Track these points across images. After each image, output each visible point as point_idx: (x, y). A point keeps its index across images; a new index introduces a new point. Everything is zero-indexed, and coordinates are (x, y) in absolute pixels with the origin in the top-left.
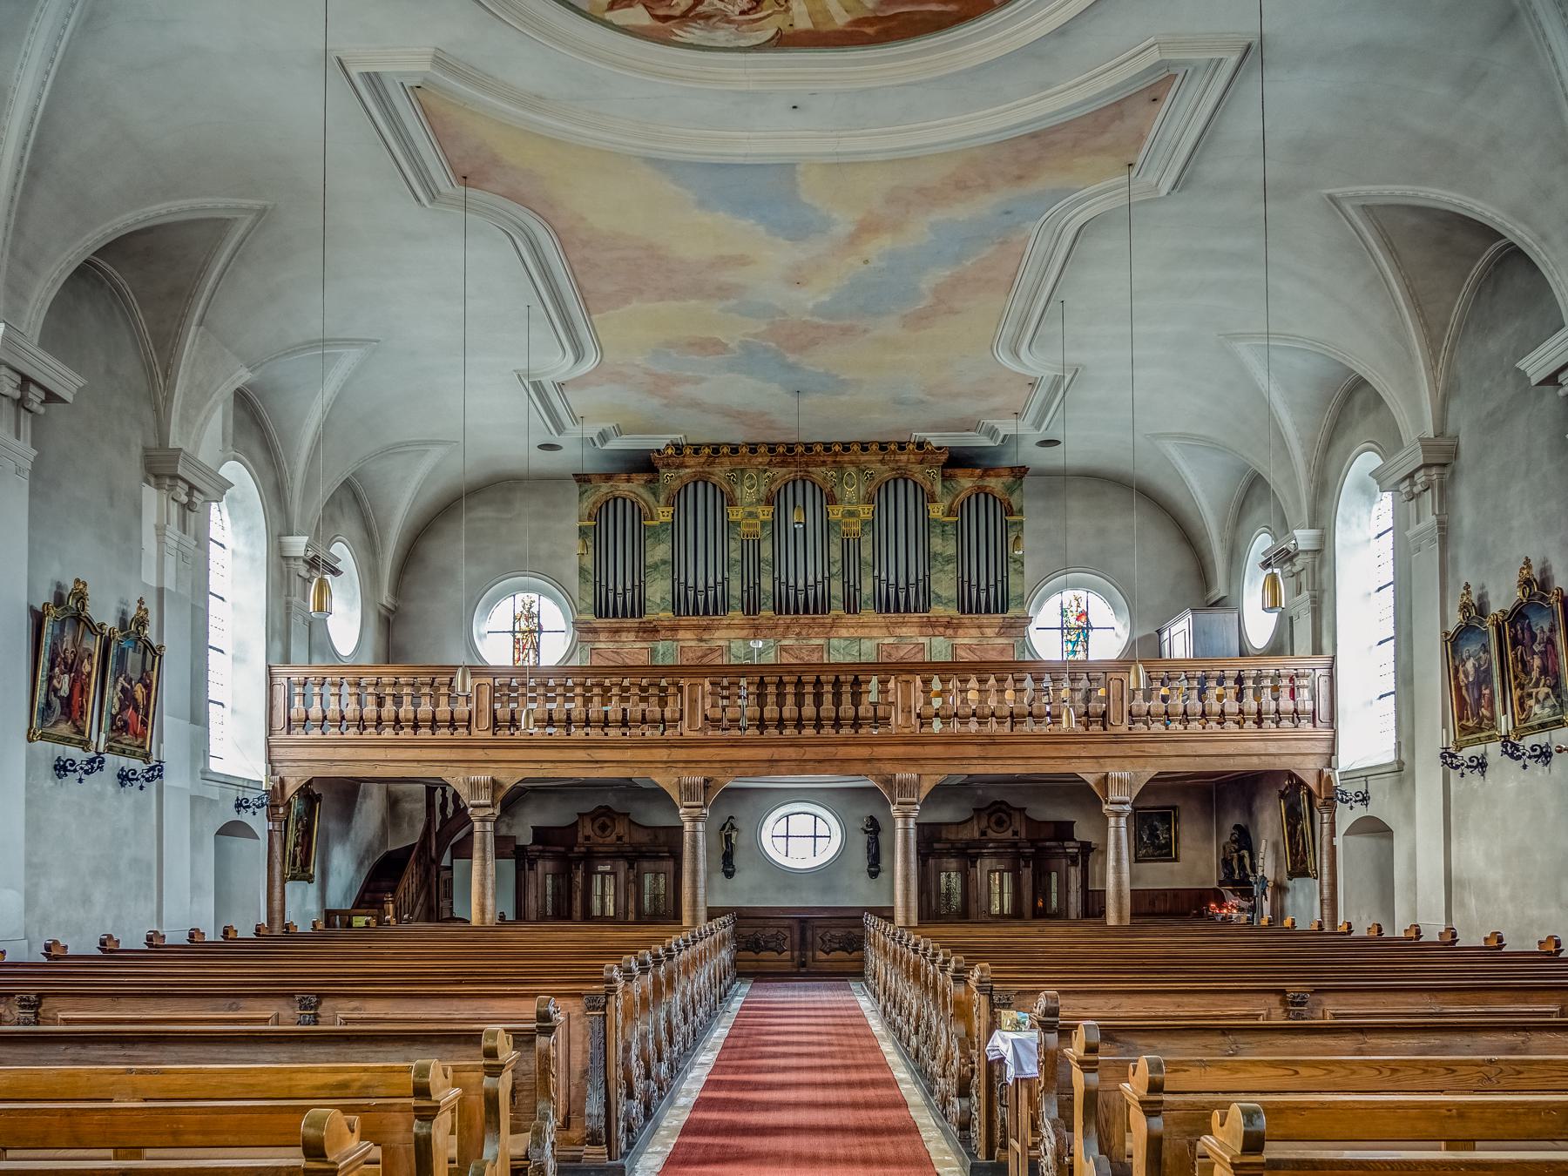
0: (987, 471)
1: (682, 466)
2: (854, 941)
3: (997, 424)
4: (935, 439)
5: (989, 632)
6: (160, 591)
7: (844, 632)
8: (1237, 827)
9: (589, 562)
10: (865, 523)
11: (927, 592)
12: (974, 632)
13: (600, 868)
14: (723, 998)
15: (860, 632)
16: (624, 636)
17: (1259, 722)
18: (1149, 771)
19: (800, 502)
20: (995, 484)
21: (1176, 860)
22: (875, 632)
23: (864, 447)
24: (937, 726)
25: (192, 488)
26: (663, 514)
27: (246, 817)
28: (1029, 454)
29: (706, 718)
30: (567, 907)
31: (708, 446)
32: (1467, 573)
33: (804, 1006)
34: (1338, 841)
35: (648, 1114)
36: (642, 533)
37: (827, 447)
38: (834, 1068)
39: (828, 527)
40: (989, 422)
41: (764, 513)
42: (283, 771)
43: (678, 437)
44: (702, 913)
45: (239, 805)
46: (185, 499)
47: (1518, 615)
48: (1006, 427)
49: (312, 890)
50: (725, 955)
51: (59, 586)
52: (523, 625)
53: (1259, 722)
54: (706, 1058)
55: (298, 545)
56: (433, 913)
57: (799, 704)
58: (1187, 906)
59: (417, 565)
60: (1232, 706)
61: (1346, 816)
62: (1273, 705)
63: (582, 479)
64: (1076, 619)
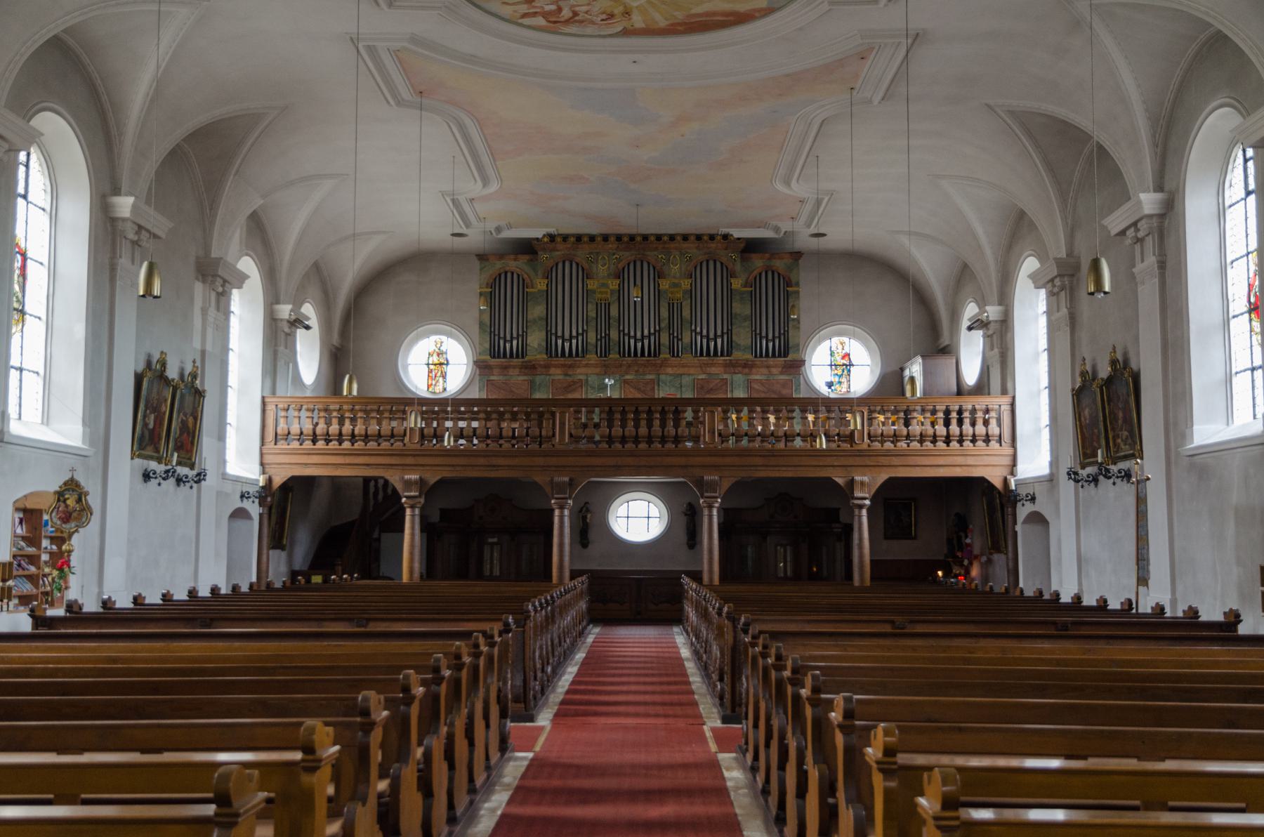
0: (773, 256)
1: (554, 250)
2: (677, 596)
3: (780, 224)
4: (737, 233)
5: (774, 371)
6: (203, 353)
7: (669, 370)
8: (957, 514)
9: (487, 319)
10: (685, 292)
11: (730, 342)
12: (764, 371)
13: (490, 540)
14: (581, 634)
15: (681, 371)
16: (511, 372)
17: (961, 442)
18: (883, 477)
19: (638, 282)
20: (779, 264)
21: (915, 538)
22: (692, 371)
23: (685, 238)
24: (732, 441)
25: (225, 281)
26: (541, 285)
27: (247, 505)
28: (804, 241)
29: (571, 435)
30: (466, 569)
31: (573, 235)
32: (1086, 351)
33: (637, 640)
34: (1018, 528)
35: (543, 692)
36: (525, 299)
37: (659, 237)
38: (653, 675)
39: (659, 294)
40: (774, 223)
41: (614, 284)
42: (271, 471)
43: (552, 230)
44: (567, 574)
45: (242, 496)
46: (220, 289)
47: (1109, 381)
48: (786, 226)
49: (283, 555)
50: (583, 605)
51: (149, 356)
52: (435, 359)
53: (961, 442)
54: (571, 671)
55: (285, 311)
56: (367, 573)
57: (637, 426)
58: (919, 572)
59: (359, 319)
60: (940, 429)
61: (1023, 511)
62: (970, 431)
63: (482, 257)
64: (840, 362)
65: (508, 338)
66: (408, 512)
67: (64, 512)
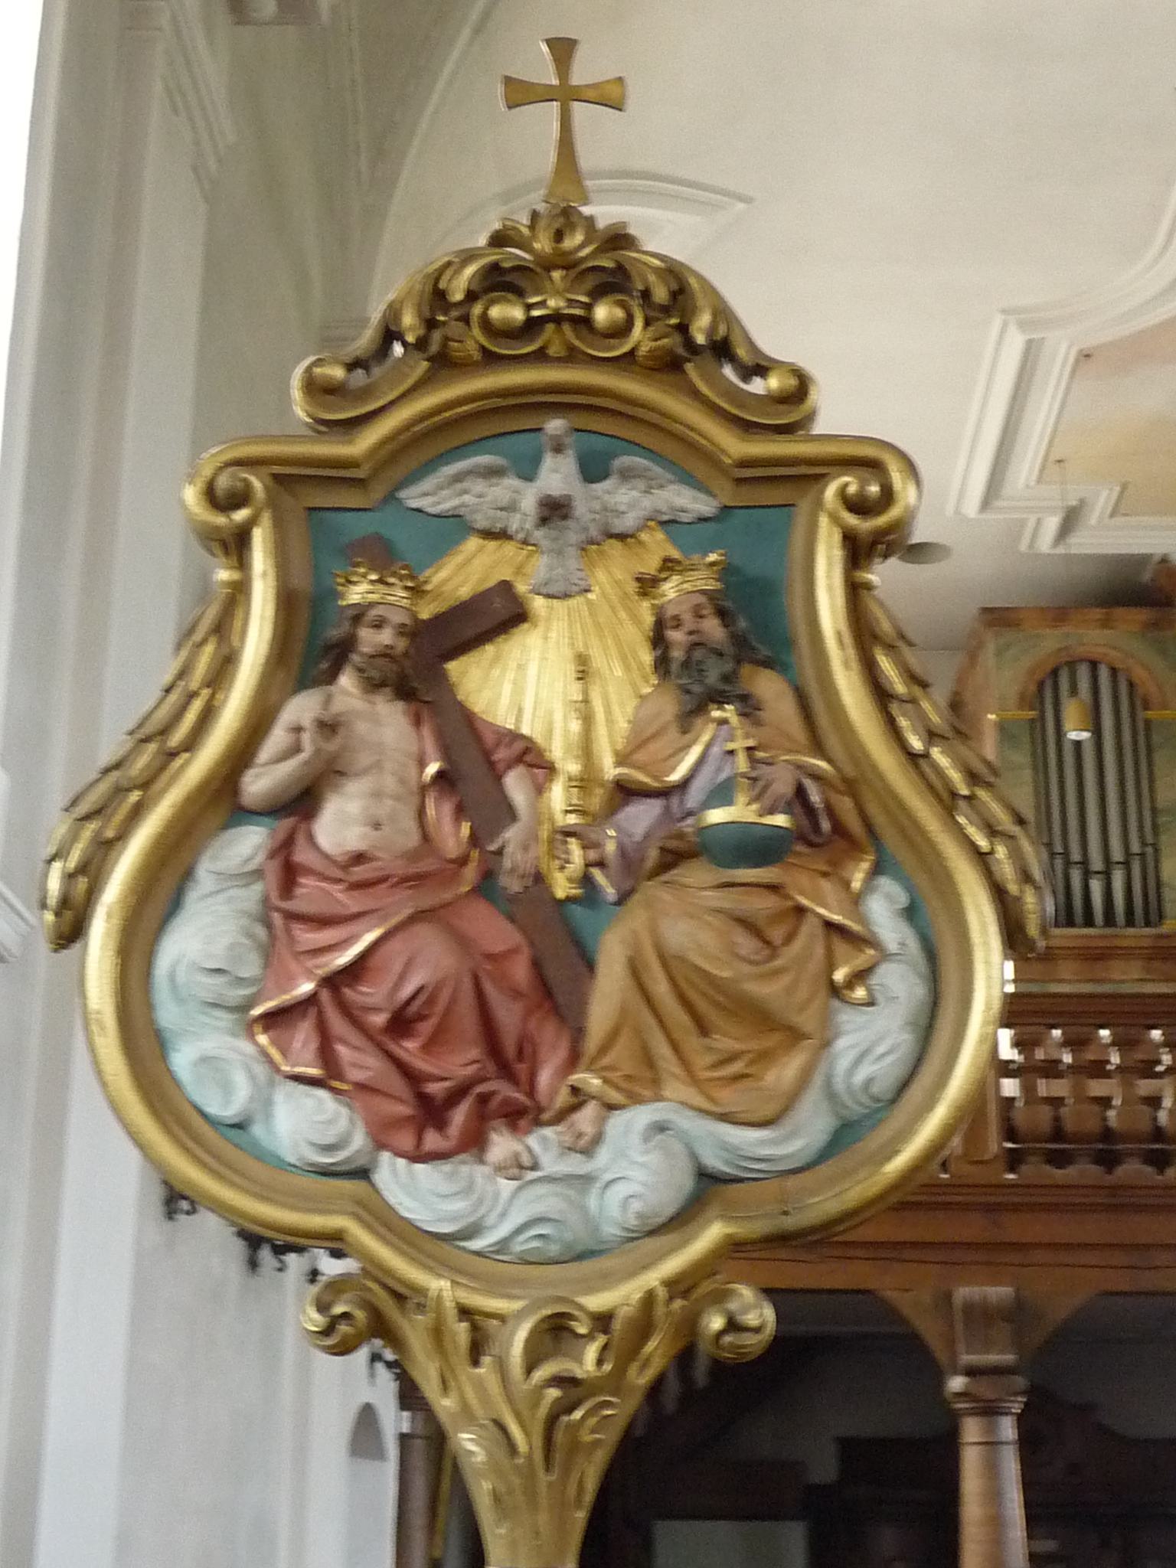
65: (1097, 864)
66: (972, 1430)
67: (419, 884)
